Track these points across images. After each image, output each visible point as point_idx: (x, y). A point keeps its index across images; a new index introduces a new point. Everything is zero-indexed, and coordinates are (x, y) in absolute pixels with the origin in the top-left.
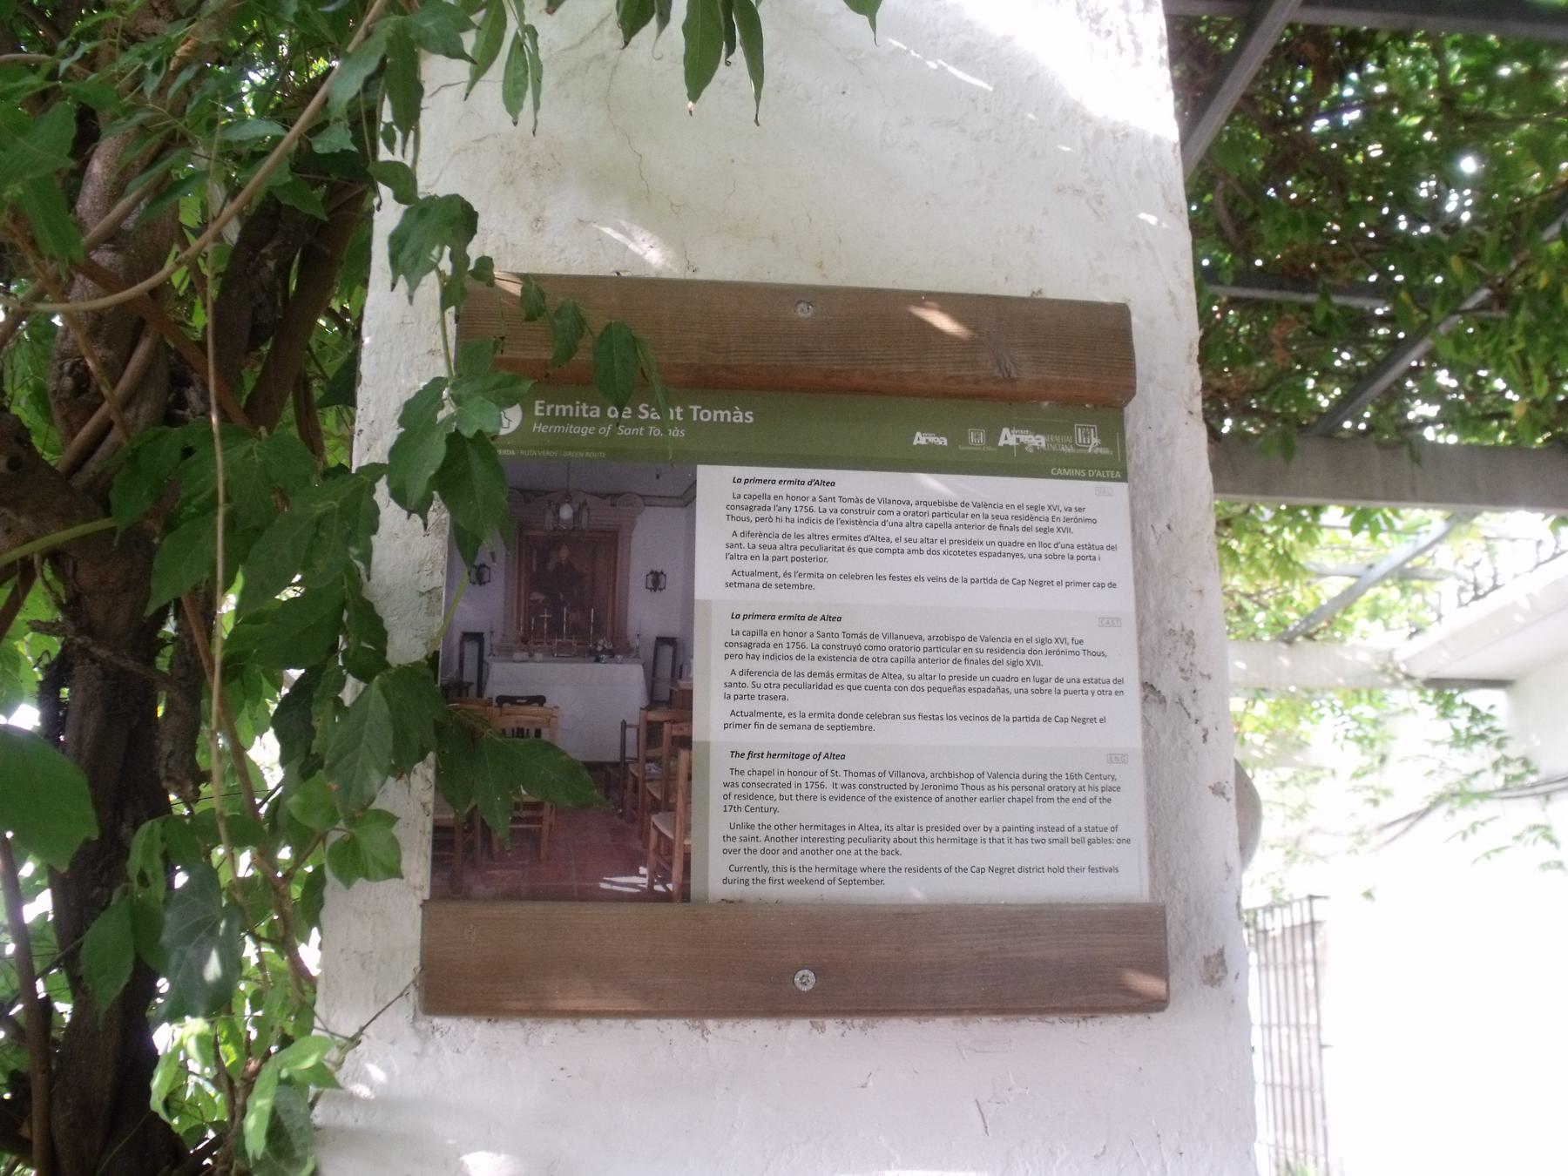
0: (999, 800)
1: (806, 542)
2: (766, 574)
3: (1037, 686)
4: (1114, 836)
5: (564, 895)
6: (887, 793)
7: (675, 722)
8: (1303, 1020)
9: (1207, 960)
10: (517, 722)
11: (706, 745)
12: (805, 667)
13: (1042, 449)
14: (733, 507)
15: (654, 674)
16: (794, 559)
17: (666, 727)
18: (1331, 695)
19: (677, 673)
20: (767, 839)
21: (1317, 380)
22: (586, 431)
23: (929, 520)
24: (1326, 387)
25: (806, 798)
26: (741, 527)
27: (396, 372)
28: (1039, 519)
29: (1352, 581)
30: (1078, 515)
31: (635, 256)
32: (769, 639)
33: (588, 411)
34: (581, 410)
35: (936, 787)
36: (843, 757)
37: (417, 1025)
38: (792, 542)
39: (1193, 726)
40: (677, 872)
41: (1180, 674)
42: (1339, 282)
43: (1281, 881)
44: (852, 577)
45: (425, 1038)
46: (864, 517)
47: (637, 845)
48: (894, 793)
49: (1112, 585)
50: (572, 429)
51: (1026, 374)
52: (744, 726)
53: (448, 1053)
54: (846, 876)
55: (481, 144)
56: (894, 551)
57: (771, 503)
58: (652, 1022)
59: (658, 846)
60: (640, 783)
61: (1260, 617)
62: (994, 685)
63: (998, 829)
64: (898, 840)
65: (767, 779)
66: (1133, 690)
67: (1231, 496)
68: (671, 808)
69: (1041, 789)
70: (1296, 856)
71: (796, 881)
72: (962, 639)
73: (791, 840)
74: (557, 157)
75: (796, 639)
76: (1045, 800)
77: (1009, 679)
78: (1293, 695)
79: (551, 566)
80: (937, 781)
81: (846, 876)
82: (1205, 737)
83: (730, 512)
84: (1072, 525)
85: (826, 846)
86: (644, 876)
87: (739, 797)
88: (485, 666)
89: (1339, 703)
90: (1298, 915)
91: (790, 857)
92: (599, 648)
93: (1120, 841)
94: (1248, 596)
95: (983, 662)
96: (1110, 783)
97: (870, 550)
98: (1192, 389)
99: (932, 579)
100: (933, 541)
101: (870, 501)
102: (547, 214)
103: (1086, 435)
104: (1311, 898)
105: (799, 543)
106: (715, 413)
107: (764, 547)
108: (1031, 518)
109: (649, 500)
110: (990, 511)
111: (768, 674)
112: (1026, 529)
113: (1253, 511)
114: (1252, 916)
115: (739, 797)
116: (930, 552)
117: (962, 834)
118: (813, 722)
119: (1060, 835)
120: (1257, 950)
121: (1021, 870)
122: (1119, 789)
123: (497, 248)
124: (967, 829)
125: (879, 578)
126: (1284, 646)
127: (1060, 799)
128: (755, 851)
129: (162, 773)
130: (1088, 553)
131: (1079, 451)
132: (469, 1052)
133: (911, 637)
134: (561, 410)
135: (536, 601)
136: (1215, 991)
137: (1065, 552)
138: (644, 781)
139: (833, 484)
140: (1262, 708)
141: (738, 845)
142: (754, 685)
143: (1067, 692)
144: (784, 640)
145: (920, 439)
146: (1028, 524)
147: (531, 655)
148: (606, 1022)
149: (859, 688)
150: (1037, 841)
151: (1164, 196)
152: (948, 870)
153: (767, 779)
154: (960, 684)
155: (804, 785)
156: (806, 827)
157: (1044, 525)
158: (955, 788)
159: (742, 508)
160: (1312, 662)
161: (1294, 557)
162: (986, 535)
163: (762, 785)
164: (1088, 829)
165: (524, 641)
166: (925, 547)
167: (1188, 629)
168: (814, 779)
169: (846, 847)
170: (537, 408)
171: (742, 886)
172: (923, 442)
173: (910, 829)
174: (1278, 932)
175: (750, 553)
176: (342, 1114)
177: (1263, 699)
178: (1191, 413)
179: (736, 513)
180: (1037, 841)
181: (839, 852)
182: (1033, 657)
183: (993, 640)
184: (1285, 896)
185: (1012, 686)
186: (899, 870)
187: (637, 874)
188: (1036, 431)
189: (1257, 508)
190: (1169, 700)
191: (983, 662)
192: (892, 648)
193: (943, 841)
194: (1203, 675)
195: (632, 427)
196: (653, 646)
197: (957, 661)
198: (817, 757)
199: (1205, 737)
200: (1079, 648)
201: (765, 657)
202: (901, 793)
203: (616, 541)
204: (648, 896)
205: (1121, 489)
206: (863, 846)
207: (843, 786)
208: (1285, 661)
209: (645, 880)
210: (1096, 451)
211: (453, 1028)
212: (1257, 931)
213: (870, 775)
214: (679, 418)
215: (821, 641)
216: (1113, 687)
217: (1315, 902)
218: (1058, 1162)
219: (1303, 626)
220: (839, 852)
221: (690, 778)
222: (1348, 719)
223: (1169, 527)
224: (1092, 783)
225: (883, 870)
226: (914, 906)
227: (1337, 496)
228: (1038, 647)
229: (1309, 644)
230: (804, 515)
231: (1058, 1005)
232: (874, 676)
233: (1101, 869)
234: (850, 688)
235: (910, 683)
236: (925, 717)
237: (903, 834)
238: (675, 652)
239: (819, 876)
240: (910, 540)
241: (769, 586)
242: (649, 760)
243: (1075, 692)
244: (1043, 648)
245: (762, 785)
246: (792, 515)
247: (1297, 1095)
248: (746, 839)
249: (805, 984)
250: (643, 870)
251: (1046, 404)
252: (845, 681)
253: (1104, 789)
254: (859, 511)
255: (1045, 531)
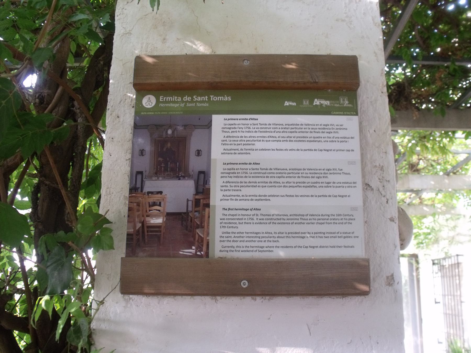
0: (313, 223)
1: (248, 139)
2: (235, 150)
3: (326, 185)
4: (353, 235)
5: (169, 256)
6: (275, 221)
7: (204, 199)
8: (455, 294)
9: (388, 278)
10: (153, 200)
11: (215, 206)
12: (248, 180)
13: (328, 106)
14: (224, 128)
15: (198, 183)
16: (244, 145)
17: (201, 200)
18: (463, 192)
19: (205, 183)
20: (234, 237)
21: (453, 90)
22: (176, 105)
23: (290, 130)
24: (456, 93)
25: (247, 223)
26: (226, 134)
27: (120, 90)
28: (327, 129)
29: (467, 155)
30: (341, 127)
31: (195, 49)
32: (236, 171)
33: (177, 99)
34: (175, 99)
35: (291, 219)
36: (260, 210)
37: (125, 298)
38: (243, 139)
39: (383, 198)
40: (204, 248)
41: (378, 180)
42: (458, 57)
43: (448, 250)
44: (263, 150)
45: (127, 301)
46: (268, 130)
47: (192, 239)
48: (277, 221)
49: (353, 150)
50: (172, 105)
51: (321, 80)
52: (227, 200)
53: (134, 306)
54: (261, 249)
55: (147, 16)
56: (278, 141)
57: (236, 126)
58: (200, 297)
59: (199, 239)
60: (193, 219)
61: (439, 167)
62: (312, 185)
63: (312, 233)
64: (278, 237)
65: (235, 217)
66: (360, 185)
67: (425, 129)
68: (203, 227)
69: (328, 219)
70: (452, 242)
71: (244, 251)
72: (301, 169)
73: (243, 237)
74: (171, 19)
75: (244, 171)
76: (329, 223)
77: (316, 183)
78: (450, 192)
79: (165, 149)
80: (292, 217)
81: (261, 249)
82: (387, 202)
83: (223, 130)
84: (338, 130)
85: (254, 239)
86: (194, 249)
87: (225, 223)
88: (143, 183)
89: (465, 194)
90: (453, 261)
91: (242, 243)
92: (180, 175)
93: (355, 237)
94: (434, 161)
95: (308, 177)
96: (351, 217)
97: (270, 141)
98: (383, 85)
99: (291, 150)
100: (291, 137)
101: (270, 124)
102: (167, 37)
103: (344, 100)
104: (457, 255)
105: (246, 139)
106: (218, 98)
107: (234, 141)
108: (324, 129)
109: (195, 127)
110: (310, 127)
111: (235, 182)
112: (323, 132)
113: (433, 134)
114: (439, 261)
115: (225, 223)
116: (290, 141)
117: (300, 235)
118: (250, 198)
119: (334, 235)
120: (441, 272)
121: (320, 247)
122: (354, 219)
123: (151, 49)
124: (302, 233)
125: (273, 150)
126: (446, 176)
127: (334, 223)
128: (230, 241)
129: (66, 218)
130: (344, 139)
131: (341, 106)
132: (140, 307)
133: (283, 169)
134: (168, 99)
135: (160, 161)
136: (390, 288)
137: (336, 140)
138: (194, 218)
139: (257, 119)
140: (440, 196)
141: (225, 239)
142: (231, 186)
143: (336, 187)
144: (240, 171)
145: (287, 103)
146: (324, 131)
147: (158, 178)
148: (184, 297)
149: (266, 186)
150: (326, 237)
151: (373, 20)
152: (295, 247)
153: (235, 217)
154: (300, 185)
155: (247, 219)
156: (248, 233)
157: (329, 131)
158: (298, 219)
159: (227, 128)
160: (456, 181)
161: (447, 148)
162: (309, 135)
163: (233, 219)
164: (343, 233)
165: (156, 173)
166: (288, 139)
167: (382, 165)
168: (250, 217)
169: (261, 239)
170: (161, 98)
171: (226, 253)
172: (288, 104)
173: (282, 233)
174: (447, 266)
175: (229, 143)
176: (101, 325)
177: (441, 193)
178: (382, 92)
179: (225, 130)
180: (326, 237)
181: (258, 241)
182: (325, 175)
183: (311, 170)
184: (449, 254)
185: (317, 185)
186: (279, 247)
187: (192, 249)
188: (326, 99)
189: (434, 132)
190: (375, 189)
191: (308, 177)
192: (277, 173)
193: (294, 237)
194: (386, 181)
195: (191, 103)
196: (197, 174)
197: (299, 177)
198: (251, 210)
199: (387, 202)
200: (341, 172)
201: (234, 177)
202: (279, 221)
203: (186, 141)
204: (195, 255)
205: (355, 118)
206: (267, 239)
207: (260, 219)
208: (447, 181)
209: (194, 251)
210: (347, 106)
211: (136, 298)
212: (441, 266)
213: (269, 215)
214: (206, 100)
215: (253, 171)
216: (353, 185)
217: (459, 257)
218: (335, 345)
219: (452, 170)
220: (258, 241)
221: (209, 217)
222: (468, 199)
223: (375, 131)
224: (345, 217)
225: (273, 247)
226: (282, 259)
227: (460, 127)
228: (327, 172)
229: (454, 176)
230: (247, 130)
231: (331, 293)
232: (271, 182)
233: (348, 247)
234: (262, 187)
235: (283, 185)
236: (288, 196)
237: (280, 235)
238: (204, 177)
239: (252, 249)
240: (283, 137)
241: (236, 153)
242: (196, 211)
243: (339, 187)
244: (329, 172)
245: (233, 219)
246: (244, 130)
247: (457, 318)
248: (227, 237)
249: (245, 285)
250: (193, 248)
251: (330, 90)
252: (261, 184)
253: (349, 219)
254: (266, 128)
255: (329, 133)
